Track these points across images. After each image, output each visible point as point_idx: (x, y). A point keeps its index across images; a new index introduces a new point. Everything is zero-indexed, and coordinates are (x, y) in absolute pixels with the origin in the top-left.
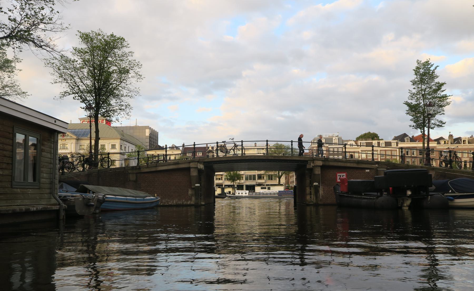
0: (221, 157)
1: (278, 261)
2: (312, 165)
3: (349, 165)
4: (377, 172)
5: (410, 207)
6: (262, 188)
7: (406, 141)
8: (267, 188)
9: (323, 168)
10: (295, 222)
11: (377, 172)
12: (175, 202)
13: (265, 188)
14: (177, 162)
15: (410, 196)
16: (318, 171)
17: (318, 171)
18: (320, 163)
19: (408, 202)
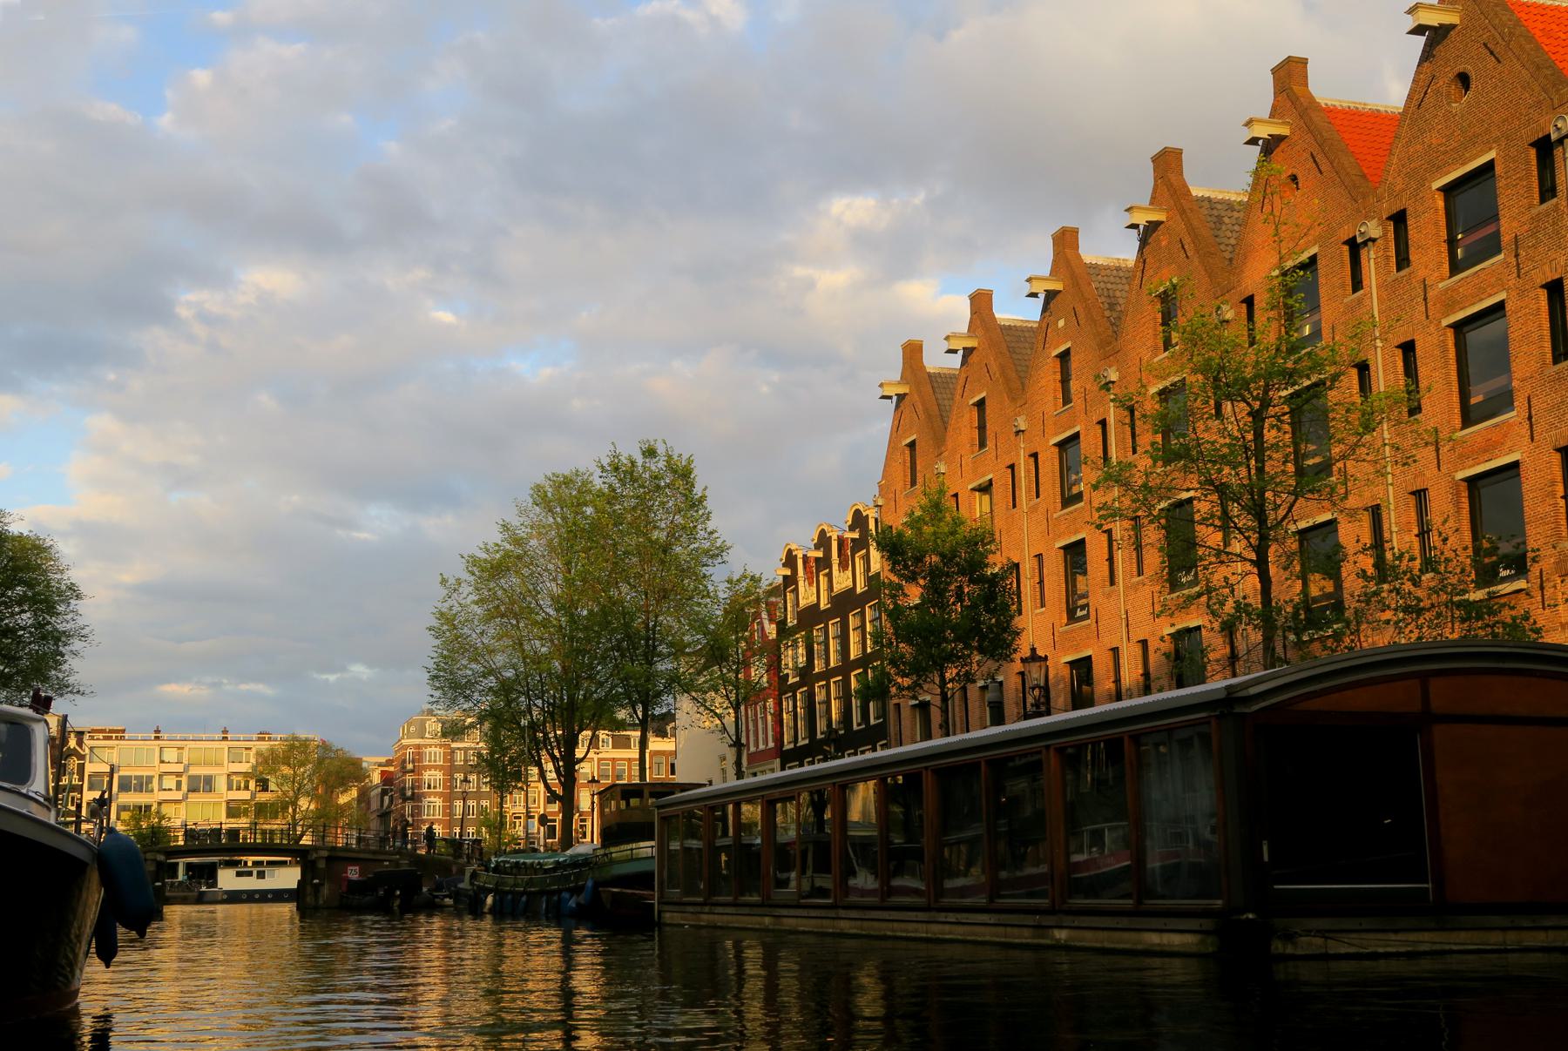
0: (794, 761)
1: (363, 1033)
2: (315, 855)
3: (362, 856)
4: (397, 864)
5: (399, 906)
6: (239, 874)
7: (983, 764)
8: (255, 873)
9: (329, 859)
10: (604, 994)
11: (397, 864)
12: (888, 996)
13: (250, 874)
14: (990, 708)
15: (399, 896)
16: (322, 865)
17: (322, 865)
18: (325, 854)
19: (397, 902)
